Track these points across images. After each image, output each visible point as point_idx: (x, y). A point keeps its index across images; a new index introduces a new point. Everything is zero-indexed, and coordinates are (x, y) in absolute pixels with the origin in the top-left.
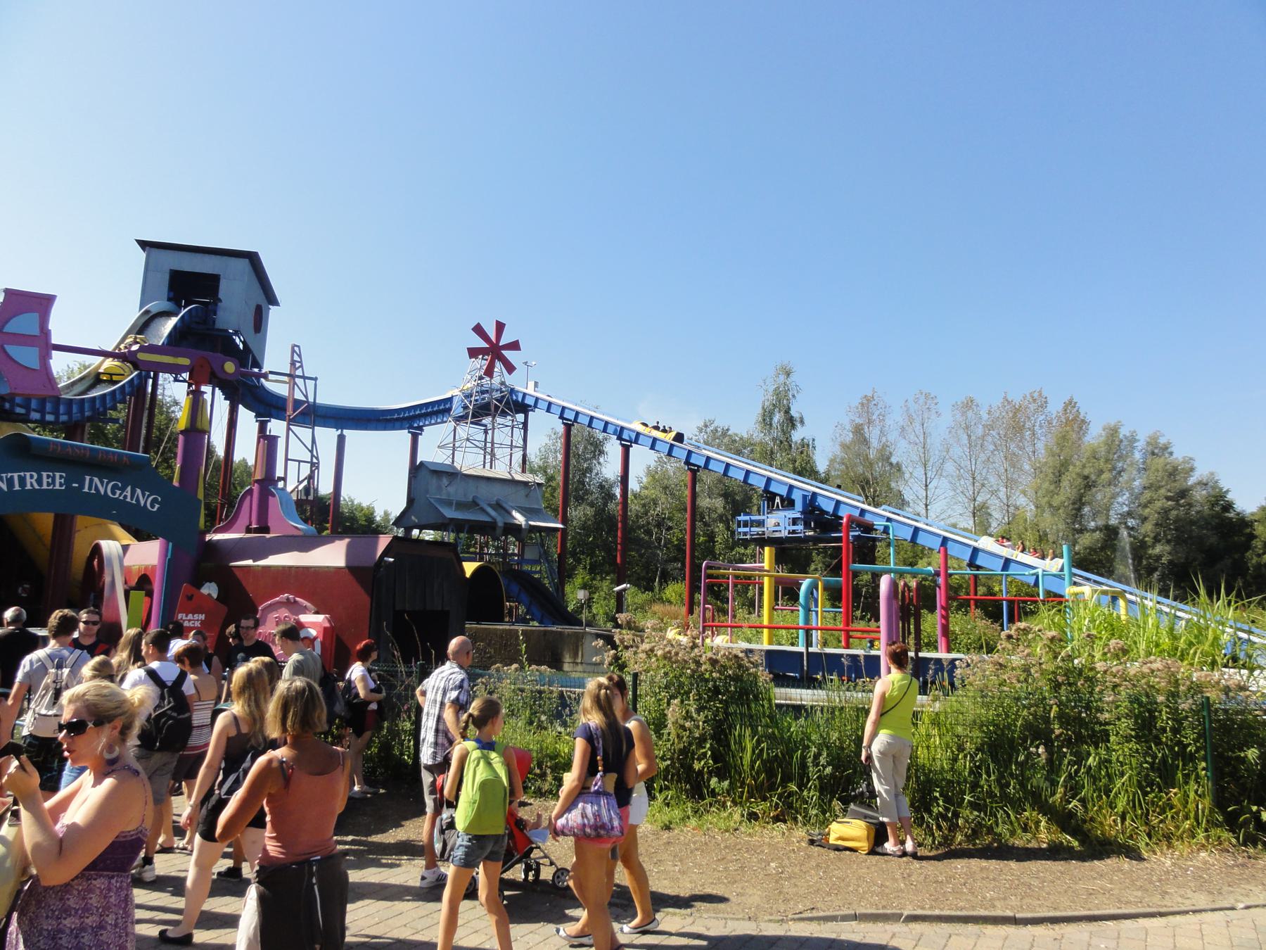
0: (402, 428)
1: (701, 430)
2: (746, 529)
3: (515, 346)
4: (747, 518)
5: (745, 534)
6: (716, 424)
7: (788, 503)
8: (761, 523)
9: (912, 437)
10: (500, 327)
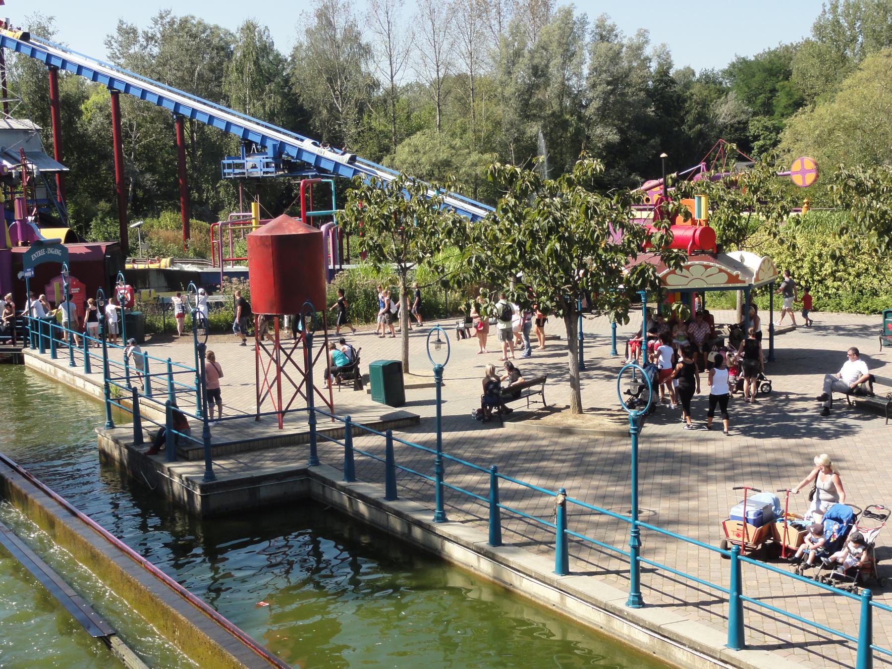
1: (156, 23)
2: (231, 171)
4: (230, 161)
5: (229, 174)
6: (172, 15)
8: (242, 166)
9: (377, 25)
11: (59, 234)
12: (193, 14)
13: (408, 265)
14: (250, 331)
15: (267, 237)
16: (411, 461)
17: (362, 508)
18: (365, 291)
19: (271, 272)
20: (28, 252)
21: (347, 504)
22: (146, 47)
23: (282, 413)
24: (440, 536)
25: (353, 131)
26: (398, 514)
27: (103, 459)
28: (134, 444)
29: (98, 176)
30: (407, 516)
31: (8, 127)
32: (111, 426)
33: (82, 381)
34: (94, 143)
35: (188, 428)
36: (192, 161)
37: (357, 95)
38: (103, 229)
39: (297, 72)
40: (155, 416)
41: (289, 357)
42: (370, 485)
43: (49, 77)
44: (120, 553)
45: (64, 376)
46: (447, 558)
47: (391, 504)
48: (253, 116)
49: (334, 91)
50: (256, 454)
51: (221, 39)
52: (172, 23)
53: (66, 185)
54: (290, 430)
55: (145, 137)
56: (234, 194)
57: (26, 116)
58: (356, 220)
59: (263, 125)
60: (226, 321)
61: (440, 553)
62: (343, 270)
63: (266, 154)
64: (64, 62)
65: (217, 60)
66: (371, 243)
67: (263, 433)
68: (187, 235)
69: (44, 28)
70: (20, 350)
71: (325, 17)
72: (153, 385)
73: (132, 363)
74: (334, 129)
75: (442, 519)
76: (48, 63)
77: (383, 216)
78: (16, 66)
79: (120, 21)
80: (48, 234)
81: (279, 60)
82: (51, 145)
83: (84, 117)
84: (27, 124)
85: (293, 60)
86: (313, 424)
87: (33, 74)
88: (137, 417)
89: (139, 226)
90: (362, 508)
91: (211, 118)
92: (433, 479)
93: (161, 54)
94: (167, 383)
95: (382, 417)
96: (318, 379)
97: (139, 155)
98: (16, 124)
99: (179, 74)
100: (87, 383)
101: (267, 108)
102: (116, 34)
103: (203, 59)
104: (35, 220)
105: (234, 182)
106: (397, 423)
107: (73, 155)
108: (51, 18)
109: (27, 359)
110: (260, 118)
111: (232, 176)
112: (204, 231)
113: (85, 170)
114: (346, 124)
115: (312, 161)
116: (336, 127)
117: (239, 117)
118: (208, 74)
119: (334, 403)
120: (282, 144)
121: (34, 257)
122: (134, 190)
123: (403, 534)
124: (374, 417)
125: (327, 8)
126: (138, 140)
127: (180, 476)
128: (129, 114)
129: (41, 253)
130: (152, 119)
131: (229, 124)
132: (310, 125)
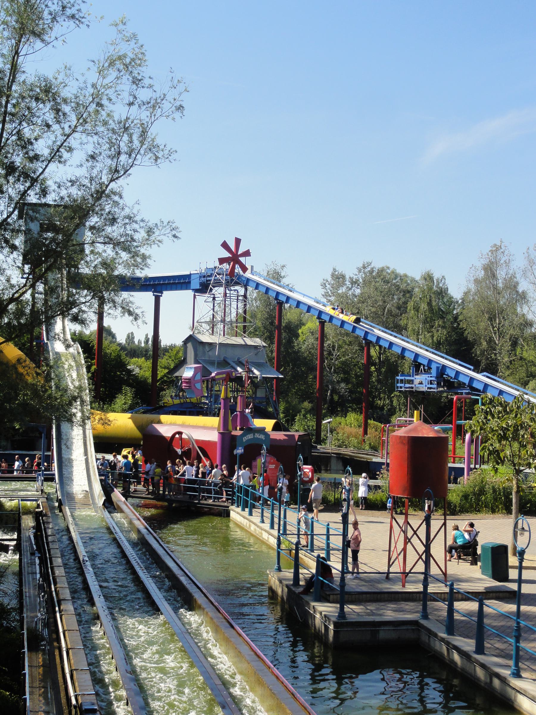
0: (146, 290)
1: (360, 271)
2: (402, 385)
3: (247, 254)
4: (403, 378)
5: (401, 387)
6: (372, 266)
7: (428, 370)
8: (411, 382)
10: (238, 241)
11: (268, 424)
12: (388, 265)
13: (522, 468)
14: (399, 510)
15: (405, 437)
16: (502, 626)
17: (456, 657)
18: (493, 487)
19: (406, 464)
20: (241, 435)
21: (446, 653)
22: (350, 289)
23: (405, 574)
24: (514, 689)
25: (506, 359)
26: (483, 666)
27: (271, 594)
28: (293, 585)
29: (306, 383)
30: (489, 668)
31: (243, 343)
32: (279, 569)
33: (267, 535)
34: (305, 358)
35: (332, 577)
36: (378, 376)
37: (511, 332)
38: (304, 423)
39: (465, 312)
40: (310, 566)
41: (415, 532)
42: (466, 640)
43: (277, 308)
44: (258, 659)
45: (255, 530)
46: (518, 708)
47: (479, 657)
48: (424, 344)
49: (493, 328)
50: (382, 604)
51: (408, 285)
52: (371, 272)
53: (281, 389)
54: (410, 588)
55: (344, 356)
56: (404, 403)
57: (257, 336)
58: (481, 429)
59: (430, 352)
60: (381, 500)
61: (513, 703)
62: (476, 469)
63: (431, 374)
64: (288, 298)
65: (403, 299)
66: (491, 449)
67: (390, 588)
68: (365, 432)
69: (278, 273)
70: (228, 507)
71: (490, 270)
72: (315, 542)
73: (303, 526)
74: (491, 357)
75: (517, 675)
76: (276, 298)
77: (502, 428)
78: (256, 299)
79: (334, 269)
80: (258, 423)
81: (451, 302)
82: (274, 358)
83: (300, 339)
84: (258, 342)
85: (462, 302)
86: (426, 587)
87: (267, 305)
88: (297, 564)
89: (329, 422)
90: (456, 657)
91: (391, 344)
92: (512, 641)
93: (362, 294)
94: (325, 542)
95: (486, 588)
96: (438, 550)
97: (338, 368)
98: (249, 342)
99: (373, 310)
100: (270, 536)
101: (435, 339)
102: (330, 279)
103: (392, 298)
104: (251, 412)
105: (405, 394)
106: (497, 594)
107: (289, 366)
108: (284, 266)
109: (232, 514)
110: (428, 346)
111: (403, 389)
112: (379, 430)
113: (298, 378)
114: (500, 353)
115: (466, 381)
116: (493, 355)
117: (413, 344)
118: (395, 311)
119: (448, 572)
120: (444, 367)
121: (245, 439)
122: (331, 395)
123: (486, 683)
124: (480, 587)
125: (492, 263)
126: (339, 358)
127: (321, 613)
128: (333, 338)
129: (250, 436)
130: (350, 342)
131: (404, 349)
132: (472, 353)
